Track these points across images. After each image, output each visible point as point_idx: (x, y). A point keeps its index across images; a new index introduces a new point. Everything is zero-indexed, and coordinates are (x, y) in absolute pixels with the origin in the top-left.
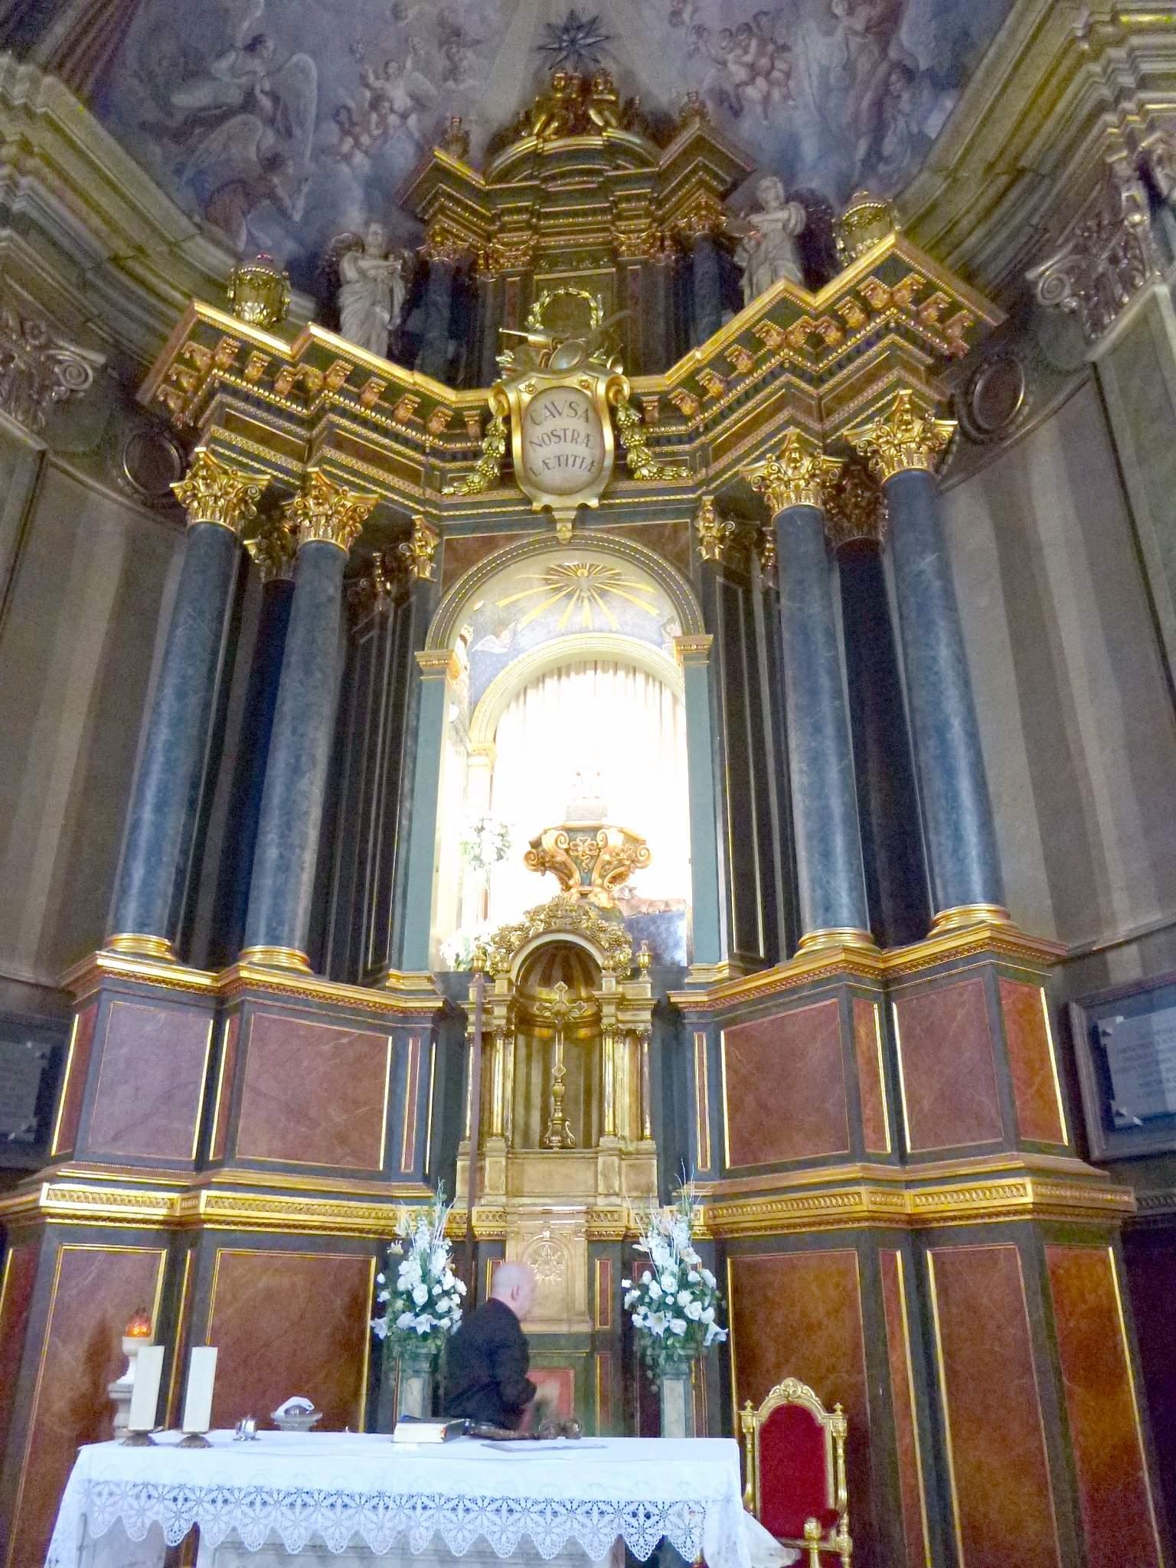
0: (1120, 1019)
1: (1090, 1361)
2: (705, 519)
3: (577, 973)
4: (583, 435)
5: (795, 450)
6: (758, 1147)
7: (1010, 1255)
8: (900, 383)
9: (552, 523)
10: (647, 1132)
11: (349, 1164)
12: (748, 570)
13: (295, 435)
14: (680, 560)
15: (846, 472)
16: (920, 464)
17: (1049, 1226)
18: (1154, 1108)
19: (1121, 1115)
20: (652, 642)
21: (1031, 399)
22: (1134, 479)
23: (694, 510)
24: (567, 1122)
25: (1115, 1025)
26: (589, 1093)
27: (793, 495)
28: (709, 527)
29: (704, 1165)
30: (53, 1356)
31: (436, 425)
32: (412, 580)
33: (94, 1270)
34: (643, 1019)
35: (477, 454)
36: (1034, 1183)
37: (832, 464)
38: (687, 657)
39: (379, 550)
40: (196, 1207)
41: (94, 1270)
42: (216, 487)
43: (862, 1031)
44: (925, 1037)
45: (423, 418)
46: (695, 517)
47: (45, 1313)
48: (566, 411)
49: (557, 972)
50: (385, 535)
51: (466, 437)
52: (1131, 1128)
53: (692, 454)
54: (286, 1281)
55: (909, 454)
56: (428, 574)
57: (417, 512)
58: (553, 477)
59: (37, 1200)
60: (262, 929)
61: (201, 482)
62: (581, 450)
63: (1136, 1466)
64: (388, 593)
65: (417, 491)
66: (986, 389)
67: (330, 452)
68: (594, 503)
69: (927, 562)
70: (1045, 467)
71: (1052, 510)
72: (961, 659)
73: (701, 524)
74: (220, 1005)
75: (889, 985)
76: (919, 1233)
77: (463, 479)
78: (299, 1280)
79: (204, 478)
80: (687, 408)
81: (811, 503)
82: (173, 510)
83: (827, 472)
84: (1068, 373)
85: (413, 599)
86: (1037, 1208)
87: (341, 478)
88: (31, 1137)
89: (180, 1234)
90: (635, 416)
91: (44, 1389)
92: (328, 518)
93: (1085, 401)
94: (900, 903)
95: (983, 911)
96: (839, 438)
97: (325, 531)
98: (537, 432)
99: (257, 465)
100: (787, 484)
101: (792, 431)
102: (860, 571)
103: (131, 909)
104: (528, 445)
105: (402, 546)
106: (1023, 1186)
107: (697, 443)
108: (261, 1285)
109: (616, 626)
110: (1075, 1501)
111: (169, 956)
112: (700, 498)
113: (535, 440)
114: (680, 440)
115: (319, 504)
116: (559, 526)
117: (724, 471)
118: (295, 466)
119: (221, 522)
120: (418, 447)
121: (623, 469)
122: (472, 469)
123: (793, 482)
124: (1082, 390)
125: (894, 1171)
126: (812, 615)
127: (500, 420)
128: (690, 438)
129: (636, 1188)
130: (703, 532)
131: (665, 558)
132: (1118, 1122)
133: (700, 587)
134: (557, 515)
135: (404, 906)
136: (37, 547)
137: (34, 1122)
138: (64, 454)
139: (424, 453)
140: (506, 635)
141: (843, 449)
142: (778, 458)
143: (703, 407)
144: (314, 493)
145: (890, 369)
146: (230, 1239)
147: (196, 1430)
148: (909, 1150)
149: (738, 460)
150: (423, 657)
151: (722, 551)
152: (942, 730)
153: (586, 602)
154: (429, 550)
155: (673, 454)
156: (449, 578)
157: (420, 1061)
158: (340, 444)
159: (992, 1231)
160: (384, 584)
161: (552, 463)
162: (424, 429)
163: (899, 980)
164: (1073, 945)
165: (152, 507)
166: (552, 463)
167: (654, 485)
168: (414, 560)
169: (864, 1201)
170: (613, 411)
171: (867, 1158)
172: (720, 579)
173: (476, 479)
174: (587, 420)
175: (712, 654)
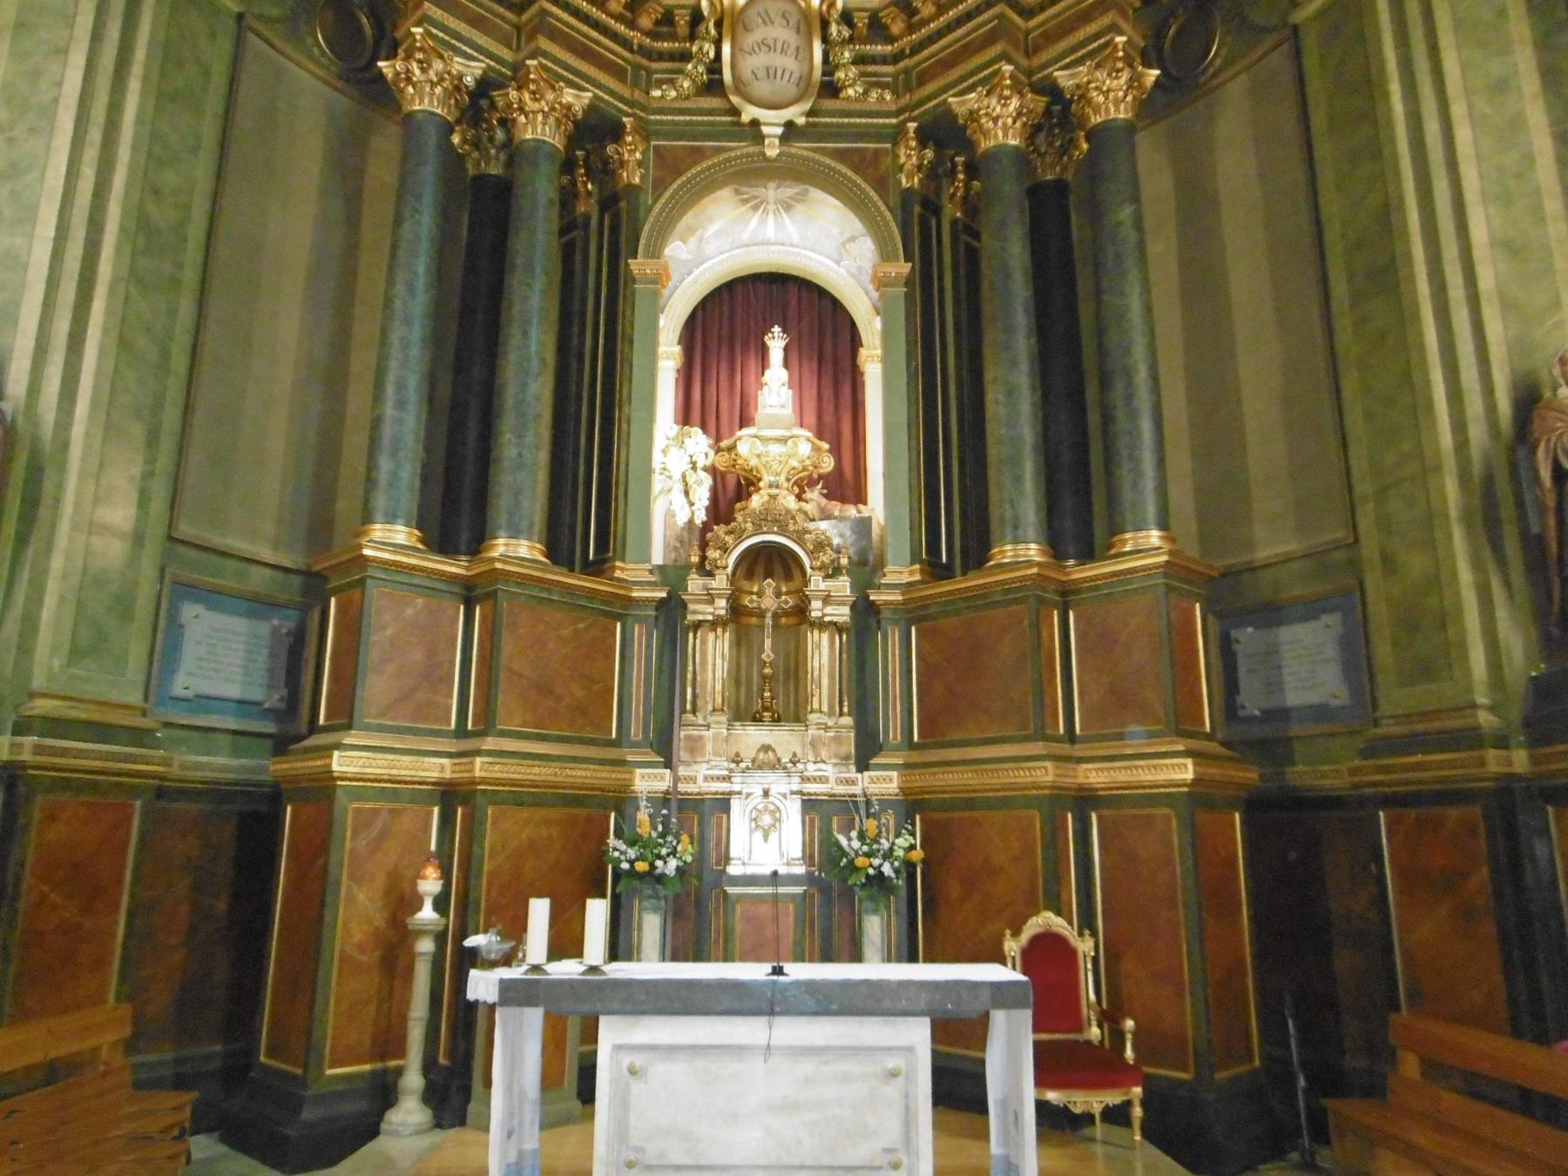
0: (1250, 630)
1: (1213, 894)
2: (907, 147)
3: (778, 569)
4: (793, 47)
5: (1007, 87)
6: (942, 719)
7: (1167, 818)
8: (1114, 29)
9: (759, 138)
10: (846, 710)
11: (588, 734)
12: (938, 196)
13: (503, 18)
14: (881, 185)
15: (1048, 112)
16: (1123, 114)
17: (1199, 797)
18: (1267, 705)
19: (1243, 707)
20: (829, 257)
21: (1223, 52)
22: (1324, 150)
23: (897, 135)
24: (770, 696)
25: (1246, 638)
26: (793, 670)
27: (1000, 134)
28: (910, 158)
29: (895, 738)
30: (351, 898)
31: (646, 22)
32: (621, 185)
33: (378, 826)
34: (841, 614)
35: (685, 57)
36: (1195, 765)
37: (1040, 103)
38: (881, 283)
39: (582, 149)
40: (471, 771)
41: (378, 826)
42: (432, 73)
43: (1045, 634)
44: (1099, 643)
45: (632, 12)
46: (895, 144)
47: (341, 863)
48: (778, 20)
49: (760, 569)
50: (594, 133)
51: (673, 37)
52: (1252, 718)
53: (895, 76)
54: (545, 832)
55: (1117, 103)
56: (637, 180)
57: (628, 115)
58: (761, 89)
59: (330, 765)
60: (503, 520)
61: (415, 65)
62: (789, 63)
63: (1244, 975)
64: (589, 193)
65: (626, 93)
66: (1178, 34)
67: (544, 43)
68: (801, 121)
69: (1125, 213)
70: (1235, 124)
71: (1236, 165)
72: (1148, 309)
73: (902, 152)
74: (470, 593)
75: (1067, 596)
76: (1084, 800)
77: (672, 82)
78: (554, 831)
79: (420, 62)
80: (896, 28)
81: (1013, 142)
82: (381, 95)
83: (1030, 111)
84: (1263, 30)
85: (623, 204)
86: (1196, 782)
87: (556, 74)
88: (282, 706)
89: (450, 795)
90: (846, 33)
91: (345, 925)
92: (546, 115)
93: (1279, 60)
94: (1079, 520)
95: (1154, 537)
96: (1045, 77)
97: (543, 130)
98: (749, 40)
99: (469, 51)
100: (995, 120)
101: (1008, 68)
102: (1048, 209)
103: (381, 501)
104: (739, 55)
105: (610, 149)
106: (1185, 766)
107: (902, 65)
108: (524, 836)
109: (796, 238)
110: (1206, 1000)
111: (420, 546)
112: (904, 123)
113: (745, 47)
114: (884, 60)
115: (536, 100)
116: (767, 141)
117: (929, 99)
118: (507, 55)
119: (439, 111)
120: (625, 43)
121: (830, 89)
122: (680, 72)
123: (1001, 121)
124: (1279, 50)
125: (1065, 749)
126: (1010, 251)
127: (711, 24)
128: (896, 58)
129: (837, 756)
130: (903, 159)
131: (865, 180)
132: (1241, 713)
133: (899, 212)
134: (765, 130)
135: (626, 504)
136: (245, 119)
137: (285, 692)
138: (260, 17)
139: (631, 51)
140: (693, 241)
141: (1052, 91)
142: (989, 93)
143: (911, 29)
144: (532, 87)
145: (1105, 11)
146: (495, 798)
147: (536, 962)
148: (1078, 731)
149: (945, 89)
150: (638, 265)
151: (920, 180)
152: (1129, 374)
153: (771, 216)
154: (638, 155)
155: (875, 75)
156: (660, 186)
157: (644, 641)
158: (554, 35)
159: (1152, 800)
160: (585, 184)
161: (761, 73)
162: (632, 25)
163: (1077, 592)
164: (1220, 563)
165: (348, 80)
166: (761, 73)
167: (857, 106)
168: (622, 164)
169: (1046, 774)
170: (825, 24)
171: (1046, 738)
172: (917, 209)
173: (686, 84)
174: (798, 31)
175: (909, 282)
